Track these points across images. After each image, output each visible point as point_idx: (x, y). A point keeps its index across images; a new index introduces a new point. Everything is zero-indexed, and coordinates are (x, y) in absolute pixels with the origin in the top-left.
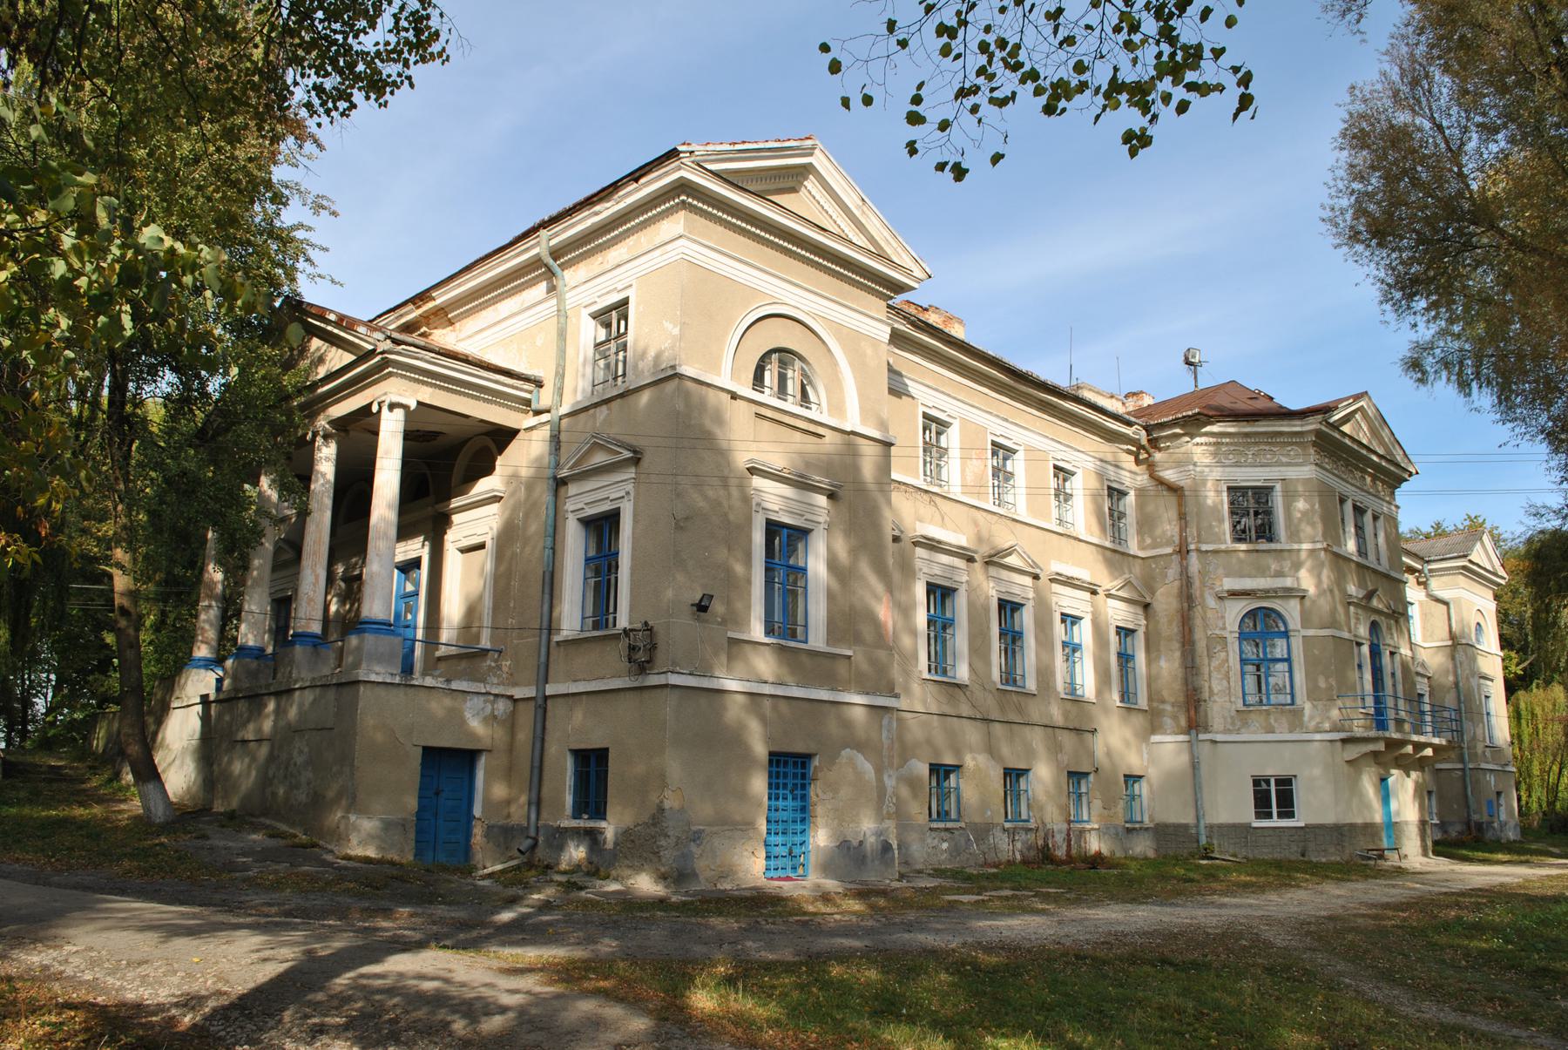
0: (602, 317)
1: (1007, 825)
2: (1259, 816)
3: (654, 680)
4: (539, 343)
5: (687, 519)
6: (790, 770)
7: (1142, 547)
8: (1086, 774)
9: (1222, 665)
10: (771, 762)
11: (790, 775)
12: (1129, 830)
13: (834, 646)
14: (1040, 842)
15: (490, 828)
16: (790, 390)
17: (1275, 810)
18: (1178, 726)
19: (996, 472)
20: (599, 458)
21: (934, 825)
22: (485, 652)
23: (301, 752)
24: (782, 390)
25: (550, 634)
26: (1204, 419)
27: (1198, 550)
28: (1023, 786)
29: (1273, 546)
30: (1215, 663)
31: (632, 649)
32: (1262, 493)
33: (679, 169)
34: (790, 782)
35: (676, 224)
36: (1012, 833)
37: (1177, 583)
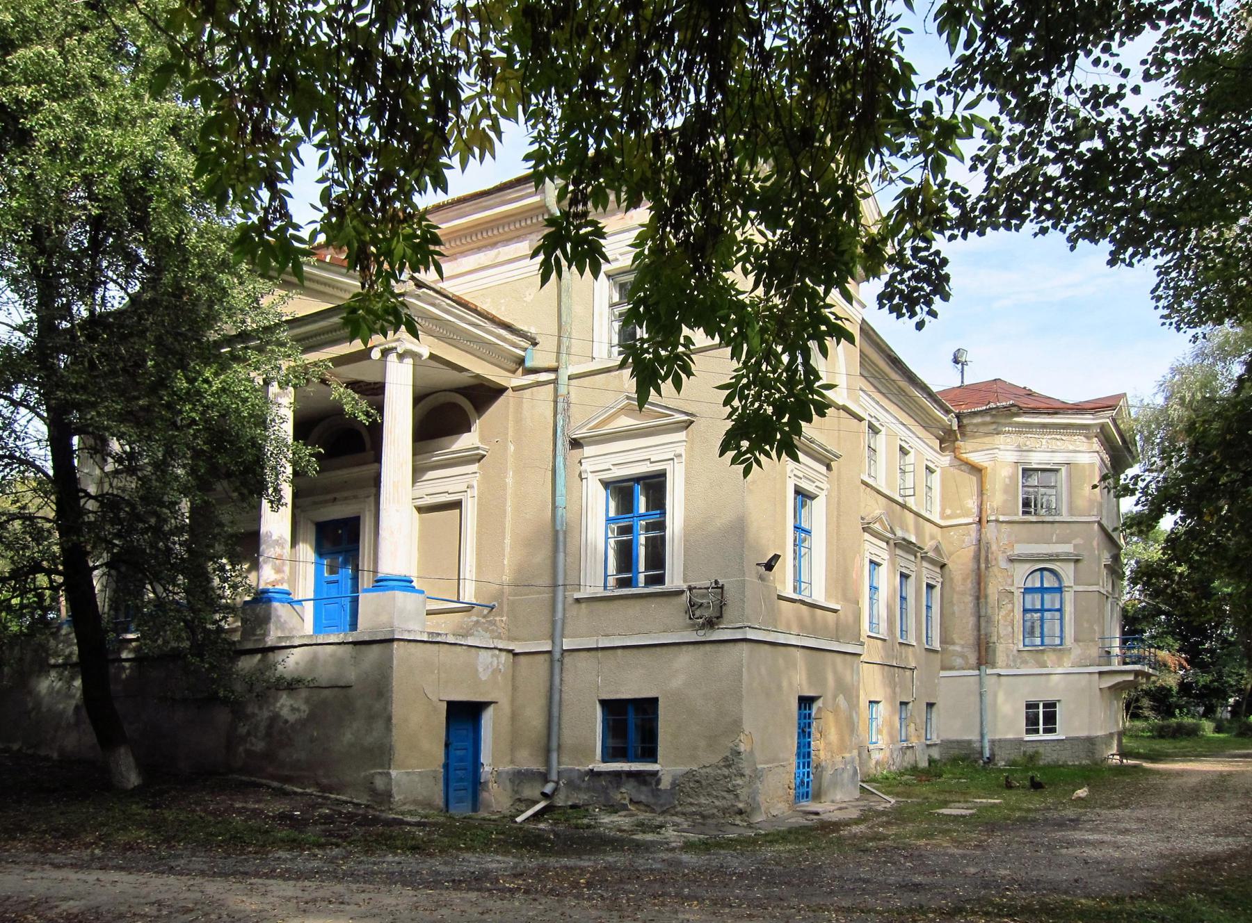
7: (943, 517)
17: (1041, 727)
30: (1003, 613)
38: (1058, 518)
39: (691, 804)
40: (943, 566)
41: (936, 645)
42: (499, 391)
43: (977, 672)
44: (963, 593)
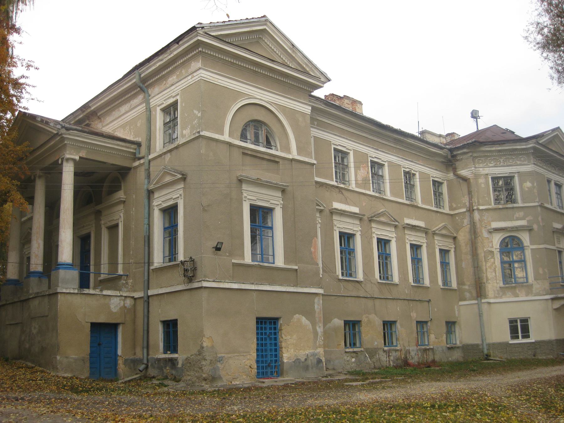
0: (166, 110)
1: (386, 348)
2: (512, 338)
3: (196, 285)
4: (139, 125)
5: (208, 206)
6: (268, 326)
7: (451, 208)
8: (426, 322)
10: (257, 322)
12: (449, 349)
14: (403, 356)
15: (126, 360)
19: (374, 174)
20: (168, 179)
22: (121, 276)
23: (35, 328)
25: (149, 266)
27: (478, 209)
28: (394, 329)
29: (515, 205)
30: (489, 264)
31: (186, 270)
32: (508, 180)
34: (268, 331)
35: (197, 64)
36: (388, 353)
37: (469, 226)
38: (515, 205)
39: (189, 375)
40: (455, 238)
41: (454, 285)
43: (476, 302)
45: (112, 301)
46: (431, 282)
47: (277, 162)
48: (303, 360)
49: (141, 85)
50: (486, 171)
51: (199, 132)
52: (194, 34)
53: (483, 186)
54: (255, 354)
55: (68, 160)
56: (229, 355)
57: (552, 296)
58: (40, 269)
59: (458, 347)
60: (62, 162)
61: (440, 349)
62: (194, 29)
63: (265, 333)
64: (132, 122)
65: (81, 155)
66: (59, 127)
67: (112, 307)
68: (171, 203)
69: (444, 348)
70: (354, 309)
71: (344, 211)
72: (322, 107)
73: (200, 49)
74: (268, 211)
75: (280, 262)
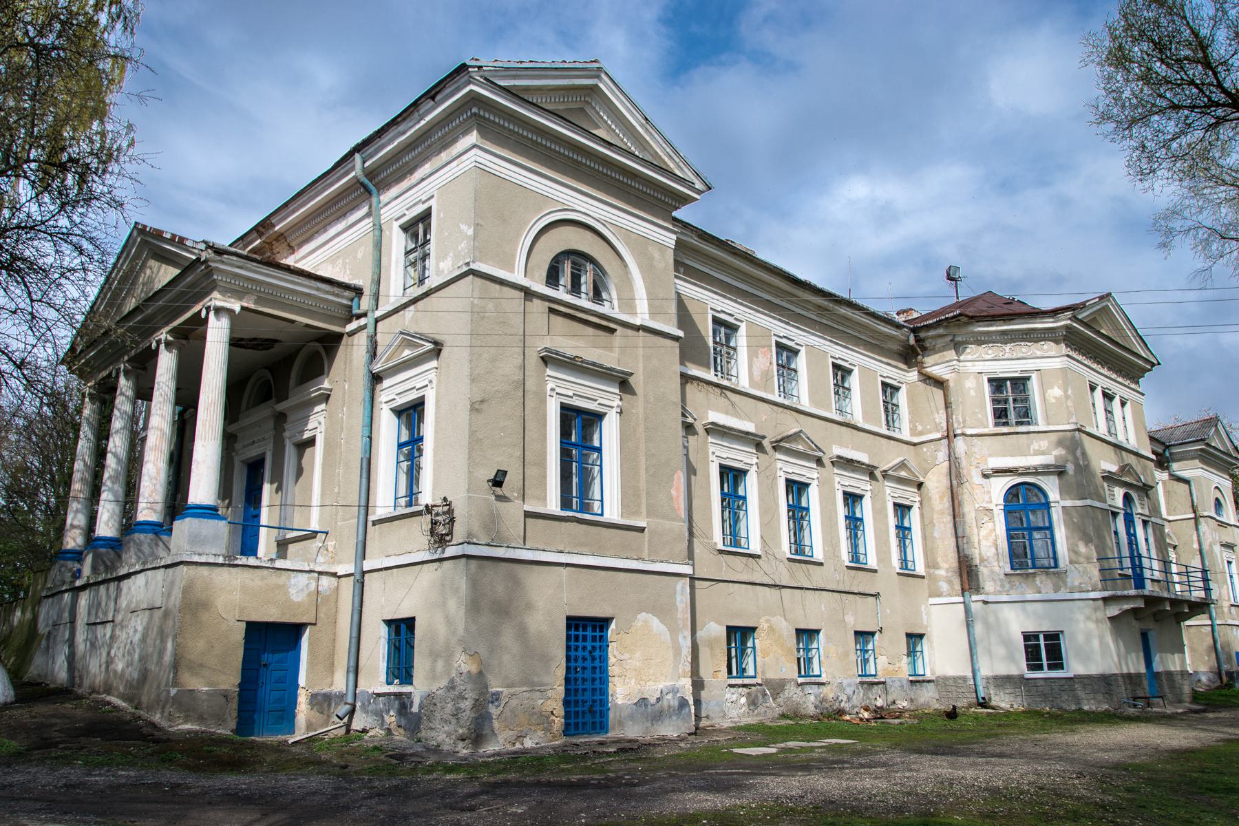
1: (800, 680)
2: (1032, 668)
5: (482, 401)
7: (914, 432)
8: (872, 634)
9: (989, 534)
10: (568, 627)
11: (589, 639)
13: (628, 518)
16: (583, 288)
18: (953, 589)
20: (407, 353)
21: (733, 681)
22: (313, 535)
24: (575, 288)
26: (964, 319)
29: (1031, 428)
30: (983, 532)
31: (434, 523)
32: (1020, 383)
33: (469, 83)
34: (589, 644)
38: (1031, 428)
40: (920, 485)
42: (340, 336)
44: (942, 513)
45: (293, 581)
46: (879, 561)
47: (612, 331)
48: (653, 700)
49: (366, 181)
50: (980, 367)
51: (468, 264)
52: (463, 80)
53: (972, 393)
54: (563, 688)
55: (218, 311)
56: (513, 690)
57: (1106, 594)
58: (154, 517)
59: (929, 681)
60: (208, 313)
61: (897, 684)
62: (463, 68)
63: (584, 648)
64: (350, 249)
65: (245, 305)
66: (203, 246)
67: (292, 591)
68: (413, 396)
69: (905, 682)
70: (744, 606)
71: (730, 429)
72: (694, 241)
73: (474, 110)
74: (593, 419)
75: (612, 513)
